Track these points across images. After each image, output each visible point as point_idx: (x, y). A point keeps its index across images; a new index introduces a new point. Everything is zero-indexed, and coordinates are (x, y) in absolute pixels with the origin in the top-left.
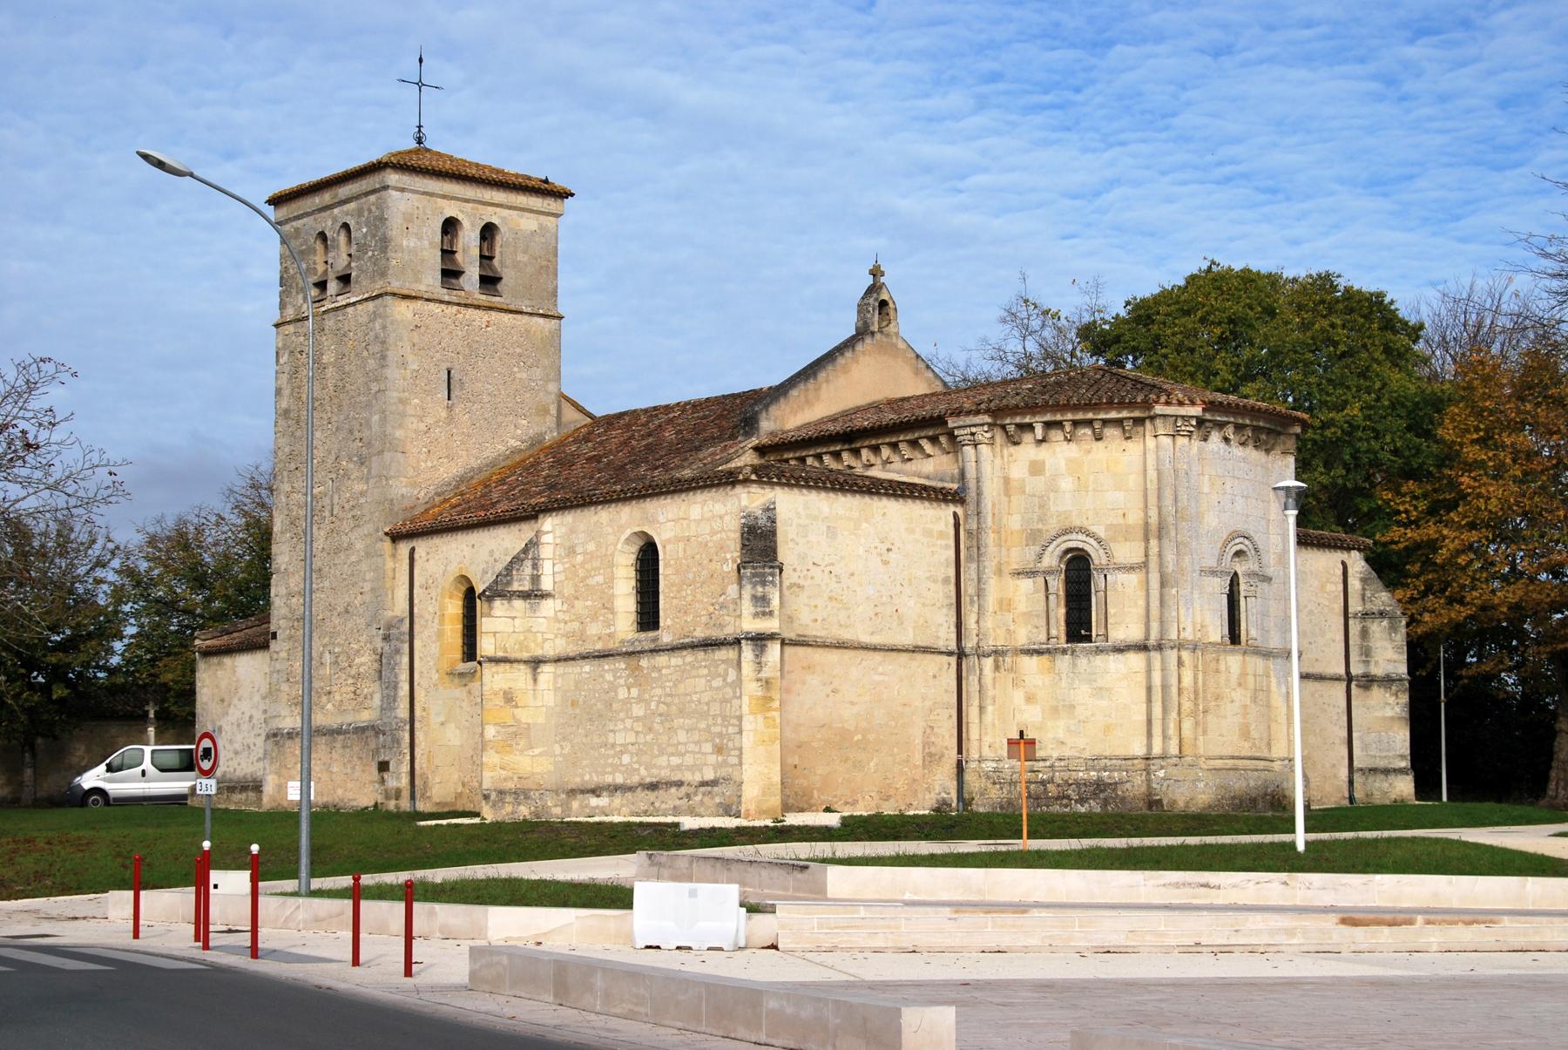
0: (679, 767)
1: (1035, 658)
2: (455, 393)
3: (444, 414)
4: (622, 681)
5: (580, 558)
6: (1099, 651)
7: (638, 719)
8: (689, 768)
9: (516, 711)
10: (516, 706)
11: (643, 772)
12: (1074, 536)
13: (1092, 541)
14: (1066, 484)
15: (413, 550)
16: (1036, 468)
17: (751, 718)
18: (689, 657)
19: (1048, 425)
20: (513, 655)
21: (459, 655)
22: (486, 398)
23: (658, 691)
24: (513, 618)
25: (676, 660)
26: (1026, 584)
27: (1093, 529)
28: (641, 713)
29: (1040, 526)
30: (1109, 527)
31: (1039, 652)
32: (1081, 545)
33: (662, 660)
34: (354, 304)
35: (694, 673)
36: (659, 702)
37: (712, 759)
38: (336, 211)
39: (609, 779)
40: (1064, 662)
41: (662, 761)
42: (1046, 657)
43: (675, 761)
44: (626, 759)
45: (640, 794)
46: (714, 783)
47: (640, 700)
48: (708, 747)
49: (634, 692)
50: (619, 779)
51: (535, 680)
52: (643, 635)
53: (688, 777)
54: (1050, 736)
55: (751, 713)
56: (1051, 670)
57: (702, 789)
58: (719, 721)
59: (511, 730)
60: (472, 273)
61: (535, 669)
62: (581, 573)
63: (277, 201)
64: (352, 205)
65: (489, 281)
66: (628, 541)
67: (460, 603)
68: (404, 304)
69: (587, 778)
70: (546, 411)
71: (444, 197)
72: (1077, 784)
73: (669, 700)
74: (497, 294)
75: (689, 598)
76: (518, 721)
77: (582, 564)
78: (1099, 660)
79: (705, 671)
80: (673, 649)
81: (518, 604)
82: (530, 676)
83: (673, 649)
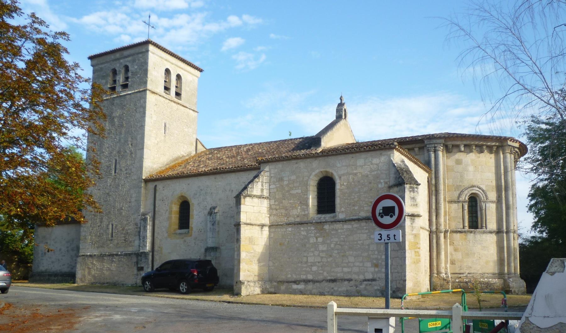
0: (348, 272)
1: (458, 234)
2: (167, 132)
3: (163, 138)
4: (313, 235)
5: (286, 183)
6: (484, 232)
7: (323, 251)
8: (355, 273)
9: (255, 247)
10: (254, 244)
11: (325, 274)
12: (475, 188)
13: (480, 190)
14: (471, 168)
15: (156, 186)
16: (459, 162)
17: (409, 251)
18: (355, 225)
19: (465, 146)
20: (253, 222)
21: (177, 227)
22: (176, 136)
23: (336, 240)
24: (254, 206)
25: (347, 226)
26: (455, 206)
27: (481, 186)
28: (325, 249)
29: (461, 184)
30: (487, 186)
31: (460, 232)
32: (477, 192)
33: (338, 226)
34: (130, 94)
35: (359, 231)
36: (335, 245)
37: (372, 269)
38: (121, 61)
39: (303, 277)
40: (471, 236)
41: (339, 269)
42: (463, 234)
43: (346, 270)
44: (314, 268)
45: (325, 284)
46: (373, 280)
47: (323, 243)
48: (369, 264)
49: (320, 240)
50: (310, 277)
51: (262, 233)
52: (319, 216)
53: (354, 277)
54: (465, 264)
55: (410, 249)
56: (465, 239)
57: (365, 283)
58: (376, 253)
59: (252, 254)
60: (173, 90)
61: (262, 228)
62: (286, 189)
63: (91, 58)
64: (130, 58)
65: (178, 94)
66: (316, 175)
67: (179, 207)
68: (153, 95)
69: (289, 276)
70: (193, 144)
71: (166, 60)
72: (480, 283)
73: (342, 243)
74: (180, 99)
75: (356, 199)
76: (255, 251)
77: (288, 185)
78: (484, 236)
79: (367, 231)
80: (345, 221)
81: (256, 200)
82: (260, 232)
83: (345, 221)
